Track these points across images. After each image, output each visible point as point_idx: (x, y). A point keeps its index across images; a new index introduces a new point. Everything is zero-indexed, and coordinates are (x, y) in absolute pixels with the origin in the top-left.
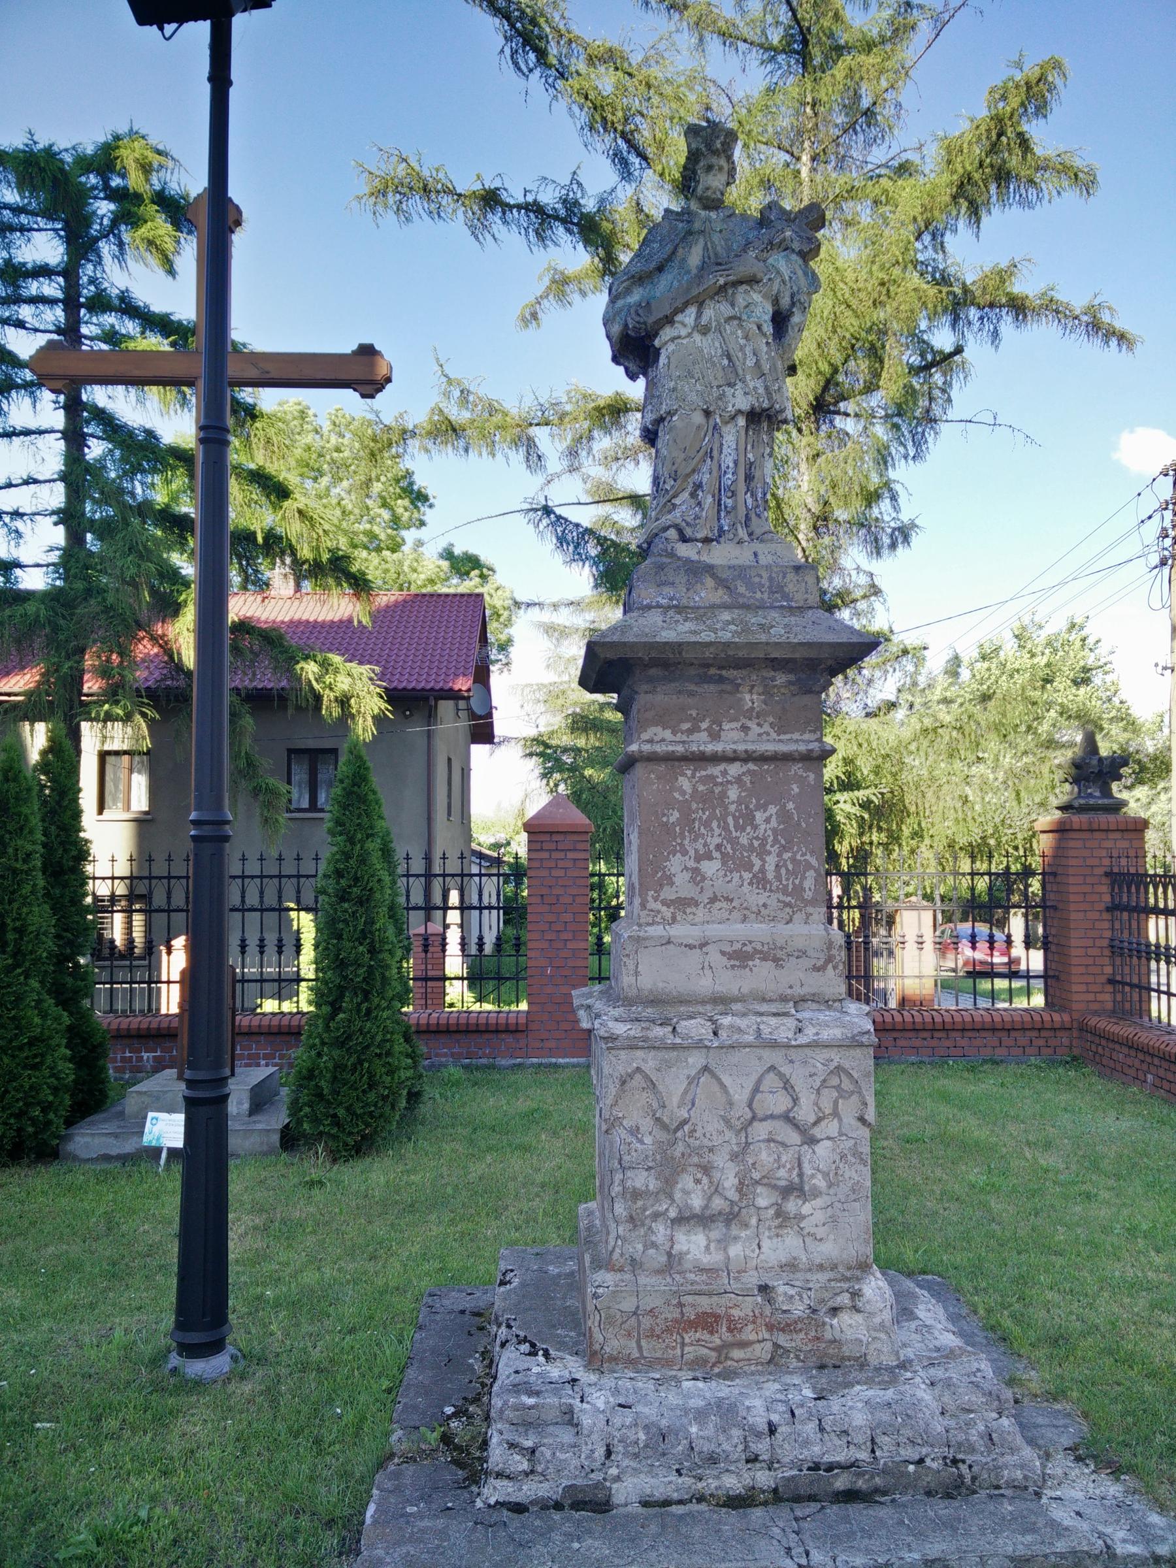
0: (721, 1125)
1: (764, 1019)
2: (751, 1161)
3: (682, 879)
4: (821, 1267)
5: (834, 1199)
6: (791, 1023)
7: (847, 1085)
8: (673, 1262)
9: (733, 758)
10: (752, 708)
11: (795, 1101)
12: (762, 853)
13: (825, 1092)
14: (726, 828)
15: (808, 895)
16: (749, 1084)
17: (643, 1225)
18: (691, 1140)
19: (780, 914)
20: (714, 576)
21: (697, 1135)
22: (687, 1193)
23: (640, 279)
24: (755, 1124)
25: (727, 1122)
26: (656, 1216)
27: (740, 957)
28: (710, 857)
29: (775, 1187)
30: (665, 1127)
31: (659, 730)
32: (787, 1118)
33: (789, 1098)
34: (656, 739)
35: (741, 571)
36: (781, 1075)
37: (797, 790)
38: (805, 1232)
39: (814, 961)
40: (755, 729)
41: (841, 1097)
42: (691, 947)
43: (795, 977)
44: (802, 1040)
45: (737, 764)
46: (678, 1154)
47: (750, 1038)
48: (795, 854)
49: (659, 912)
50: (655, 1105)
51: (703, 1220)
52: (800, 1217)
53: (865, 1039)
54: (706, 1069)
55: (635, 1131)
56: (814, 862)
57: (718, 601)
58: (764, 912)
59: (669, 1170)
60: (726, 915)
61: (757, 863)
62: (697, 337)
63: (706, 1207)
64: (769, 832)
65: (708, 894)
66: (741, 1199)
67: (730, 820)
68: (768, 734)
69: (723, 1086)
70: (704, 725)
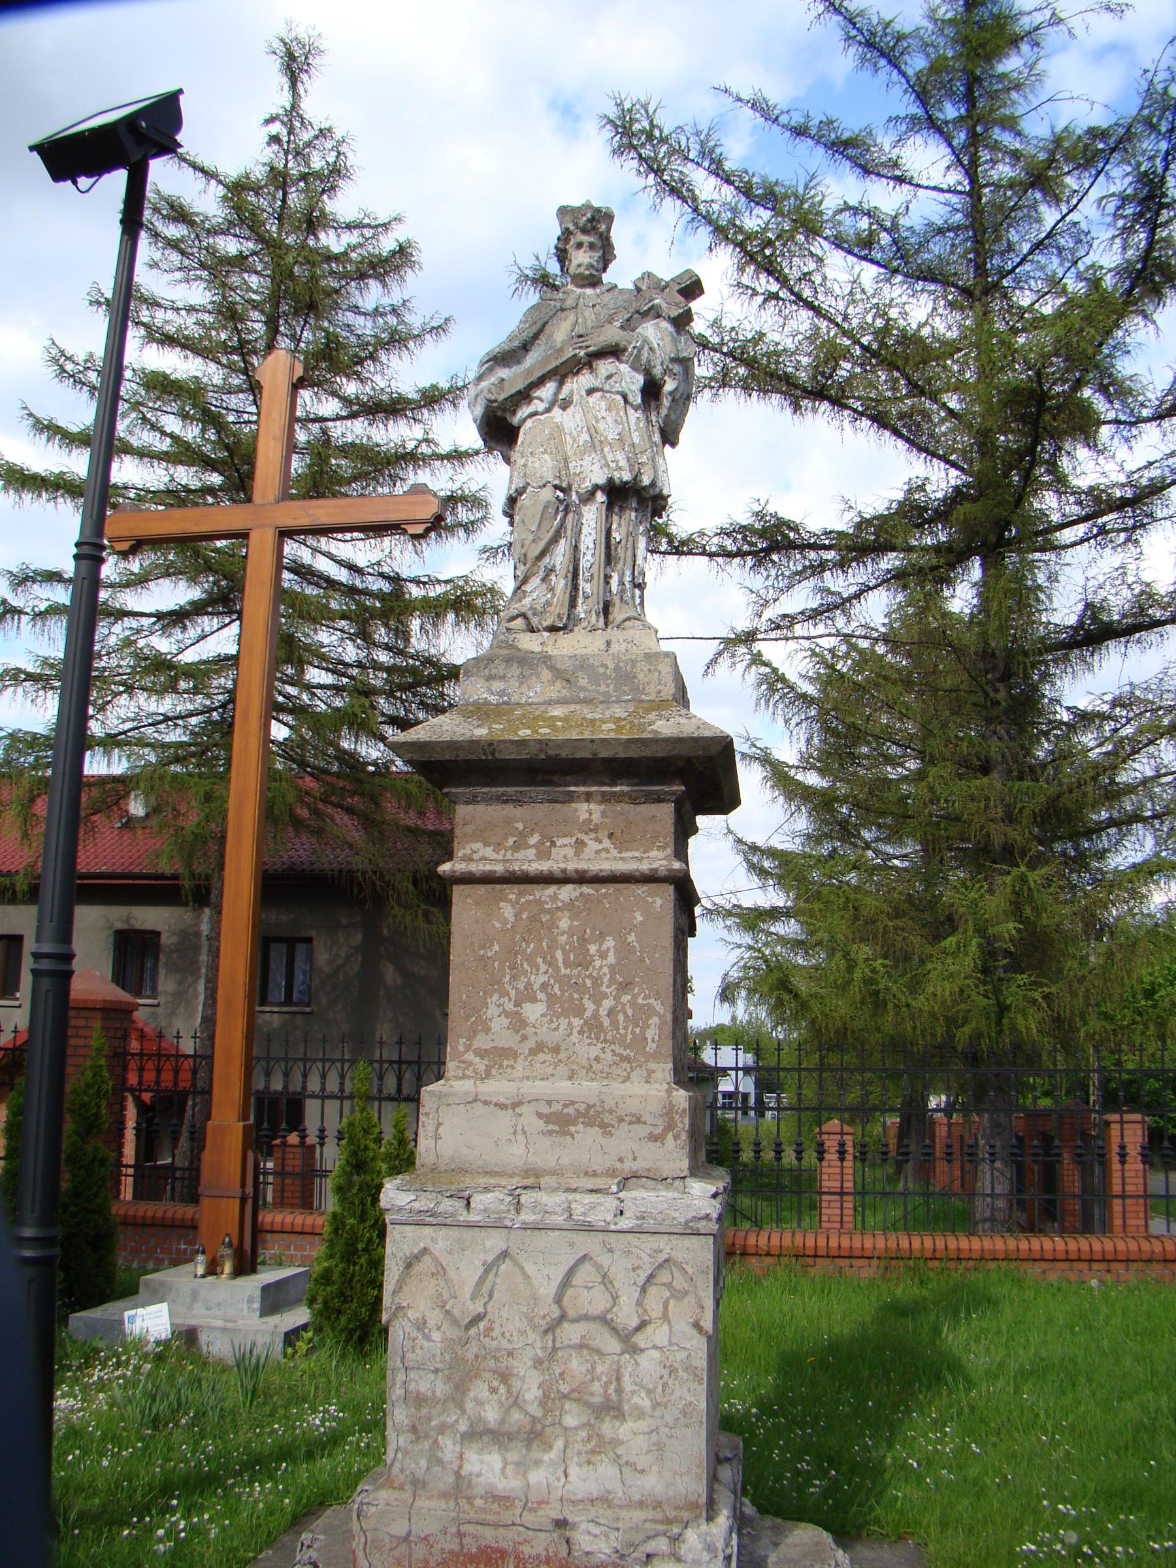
0: (524, 1325)
1: (578, 1196)
2: (557, 1371)
3: (499, 1024)
4: (641, 1504)
5: (660, 1422)
6: (611, 1203)
7: (679, 1283)
8: (460, 1487)
9: (564, 879)
10: (590, 821)
11: (615, 1299)
12: (598, 999)
13: (652, 1290)
14: (552, 963)
15: (651, 1047)
16: (558, 1275)
17: (427, 1437)
18: (487, 1340)
19: (615, 1070)
20: (552, 668)
21: (494, 1334)
22: (479, 1403)
23: (503, 359)
24: (566, 1325)
25: (531, 1320)
26: (442, 1429)
27: (561, 1121)
28: (534, 1000)
29: (588, 1404)
30: (455, 1321)
31: (477, 846)
32: (604, 1320)
33: (608, 1295)
34: (476, 857)
35: (583, 664)
36: (598, 1267)
37: (640, 918)
38: (622, 1462)
39: (649, 1129)
40: (593, 846)
41: (672, 1296)
42: (503, 1107)
43: (628, 1147)
44: (625, 1223)
45: (570, 887)
46: (470, 1356)
47: (559, 1219)
48: (635, 997)
49: (471, 1063)
50: (446, 1295)
51: (498, 1437)
52: (616, 1442)
53: (702, 1226)
54: (505, 1254)
55: (421, 1325)
56: (659, 1007)
57: (555, 695)
58: (597, 1067)
59: (461, 1375)
60: (550, 1070)
61: (590, 1007)
62: (557, 411)
63: (502, 1422)
64: (605, 970)
65: (531, 1043)
66: (545, 1416)
67: (559, 954)
68: (607, 850)
69: (527, 1277)
70: (534, 840)
